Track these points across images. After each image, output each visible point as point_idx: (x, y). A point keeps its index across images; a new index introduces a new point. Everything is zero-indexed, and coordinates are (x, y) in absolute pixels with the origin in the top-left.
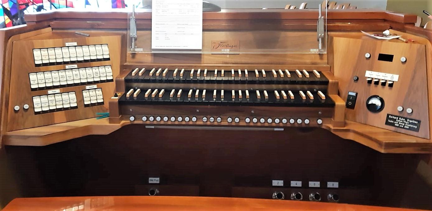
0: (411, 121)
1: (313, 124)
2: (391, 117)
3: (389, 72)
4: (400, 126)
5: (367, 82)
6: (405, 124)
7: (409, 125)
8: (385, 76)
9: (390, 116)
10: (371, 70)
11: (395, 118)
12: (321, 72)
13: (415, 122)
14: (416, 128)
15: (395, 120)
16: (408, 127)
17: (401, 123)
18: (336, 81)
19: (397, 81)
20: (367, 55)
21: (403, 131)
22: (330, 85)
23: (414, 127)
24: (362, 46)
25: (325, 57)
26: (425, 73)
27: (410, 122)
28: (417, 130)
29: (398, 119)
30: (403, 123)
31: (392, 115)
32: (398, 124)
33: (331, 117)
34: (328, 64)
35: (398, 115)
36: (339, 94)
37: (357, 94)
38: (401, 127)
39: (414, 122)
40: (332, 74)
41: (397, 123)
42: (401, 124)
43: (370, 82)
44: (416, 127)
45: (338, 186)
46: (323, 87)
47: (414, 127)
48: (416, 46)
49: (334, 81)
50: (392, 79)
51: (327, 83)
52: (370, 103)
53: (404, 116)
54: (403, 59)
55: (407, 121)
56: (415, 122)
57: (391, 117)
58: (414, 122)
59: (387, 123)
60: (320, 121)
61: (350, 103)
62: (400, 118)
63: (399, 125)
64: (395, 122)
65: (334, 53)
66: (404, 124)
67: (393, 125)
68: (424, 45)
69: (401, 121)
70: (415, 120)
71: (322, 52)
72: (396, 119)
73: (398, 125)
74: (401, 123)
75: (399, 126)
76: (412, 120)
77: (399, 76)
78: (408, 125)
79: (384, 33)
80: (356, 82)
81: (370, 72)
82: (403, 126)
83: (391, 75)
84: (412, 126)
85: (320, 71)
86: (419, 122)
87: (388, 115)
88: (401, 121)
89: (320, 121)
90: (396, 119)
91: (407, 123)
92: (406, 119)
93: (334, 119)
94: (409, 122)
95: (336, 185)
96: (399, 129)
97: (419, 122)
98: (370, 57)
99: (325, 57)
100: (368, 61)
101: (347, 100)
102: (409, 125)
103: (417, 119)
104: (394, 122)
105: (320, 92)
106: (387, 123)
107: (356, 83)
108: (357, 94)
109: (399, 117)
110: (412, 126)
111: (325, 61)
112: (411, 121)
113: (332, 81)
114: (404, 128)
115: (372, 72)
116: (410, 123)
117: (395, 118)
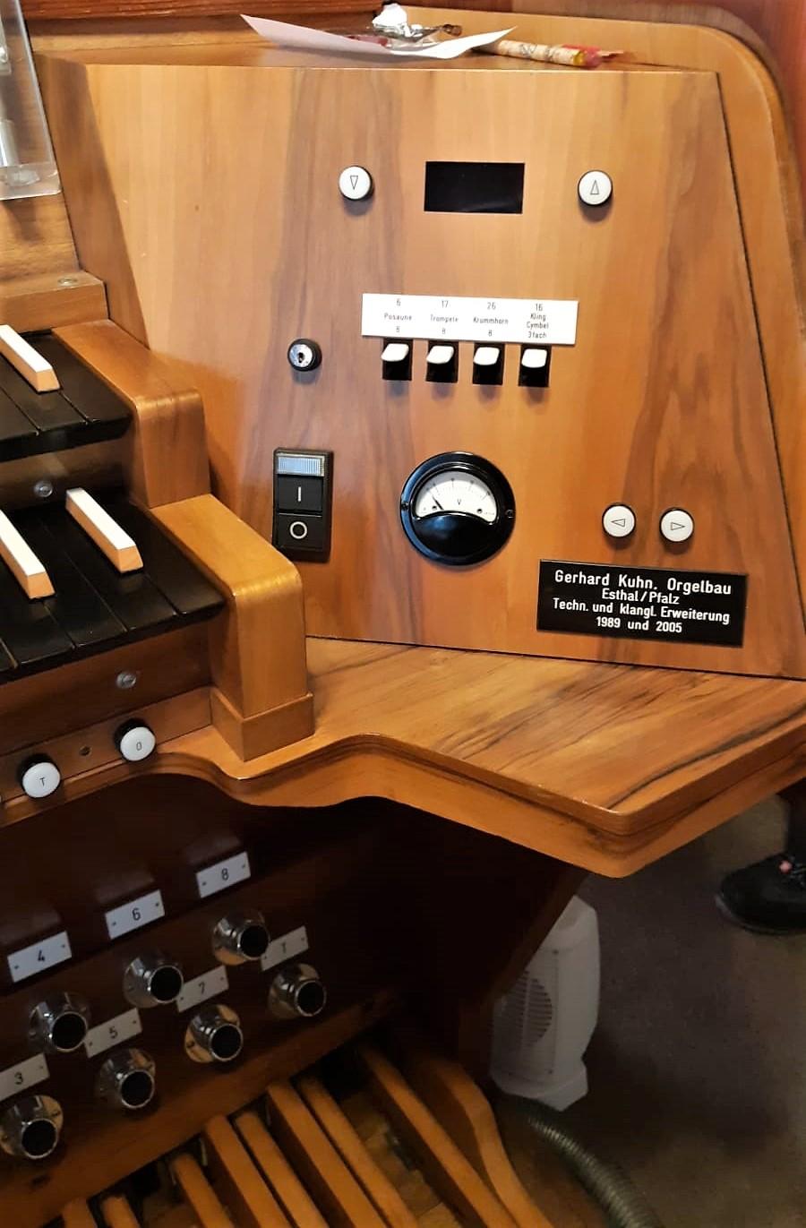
0: (689, 588)
1: (92, 769)
2: (568, 578)
3: (511, 290)
4: (631, 626)
5: (380, 373)
6: (658, 606)
7: (684, 614)
8: (491, 314)
9: (559, 577)
10: (392, 284)
11: (592, 580)
12: (49, 332)
13: (719, 589)
14: (727, 622)
15: (592, 594)
16: (677, 628)
17: (633, 604)
18: (182, 399)
19: (570, 339)
20: (354, 183)
21: (648, 651)
22: (144, 443)
23: (713, 617)
24: (303, 128)
25: (53, 220)
26: (737, 271)
27: (687, 592)
28: (730, 637)
29: (614, 586)
30: (646, 604)
31: (570, 568)
32: (616, 614)
33: (205, 681)
34: (81, 267)
35: (606, 557)
36: (216, 487)
37: (330, 459)
38: (638, 634)
39: (707, 587)
40: (135, 343)
41: (610, 607)
42: (634, 611)
43: (398, 372)
44: (726, 619)
45: (57, 383)
46: (93, 453)
47: (713, 617)
48: (655, 86)
49: (168, 402)
50: (538, 331)
51: (120, 423)
52: (425, 508)
53: (641, 565)
54: (595, 187)
55: (666, 592)
56: (719, 589)
57: (568, 578)
58: (707, 587)
59: (549, 620)
60: (137, 743)
61: (299, 530)
62: (622, 580)
63: (626, 619)
64: (596, 609)
65: (117, 188)
66: (649, 612)
67: (583, 624)
68: (711, 75)
69: (633, 597)
70: (716, 578)
71: (25, 187)
72: (600, 586)
73: (617, 623)
74: (633, 604)
75: (624, 624)
76: (695, 577)
77: (579, 305)
78: (676, 614)
79: (378, 21)
80: (308, 382)
81: (392, 298)
82: (646, 626)
83: (528, 306)
84: (700, 616)
85: (35, 325)
86: (738, 582)
87: (547, 569)
88: (633, 597)
89: (137, 743)
90: (600, 586)
91: (666, 600)
92: (660, 578)
93: (239, 704)
94: (679, 593)
95: (238, 868)
96: (624, 643)
97: (738, 582)
98: (370, 195)
99: (53, 220)
100: (361, 224)
101: (277, 509)
102: (684, 614)
103: (725, 568)
104: (589, 606)
105: (83, 502)
106: (549, 620)
107: (311, 389)
108: (330, 459)
109: (615, 572)
110: (700, 616)
111: (59, 244)
112: (689, 588)
113: (160, 409)
114: (652, 634)
115: (403, 298)
116: (687, 602)
117: (592, 580)
